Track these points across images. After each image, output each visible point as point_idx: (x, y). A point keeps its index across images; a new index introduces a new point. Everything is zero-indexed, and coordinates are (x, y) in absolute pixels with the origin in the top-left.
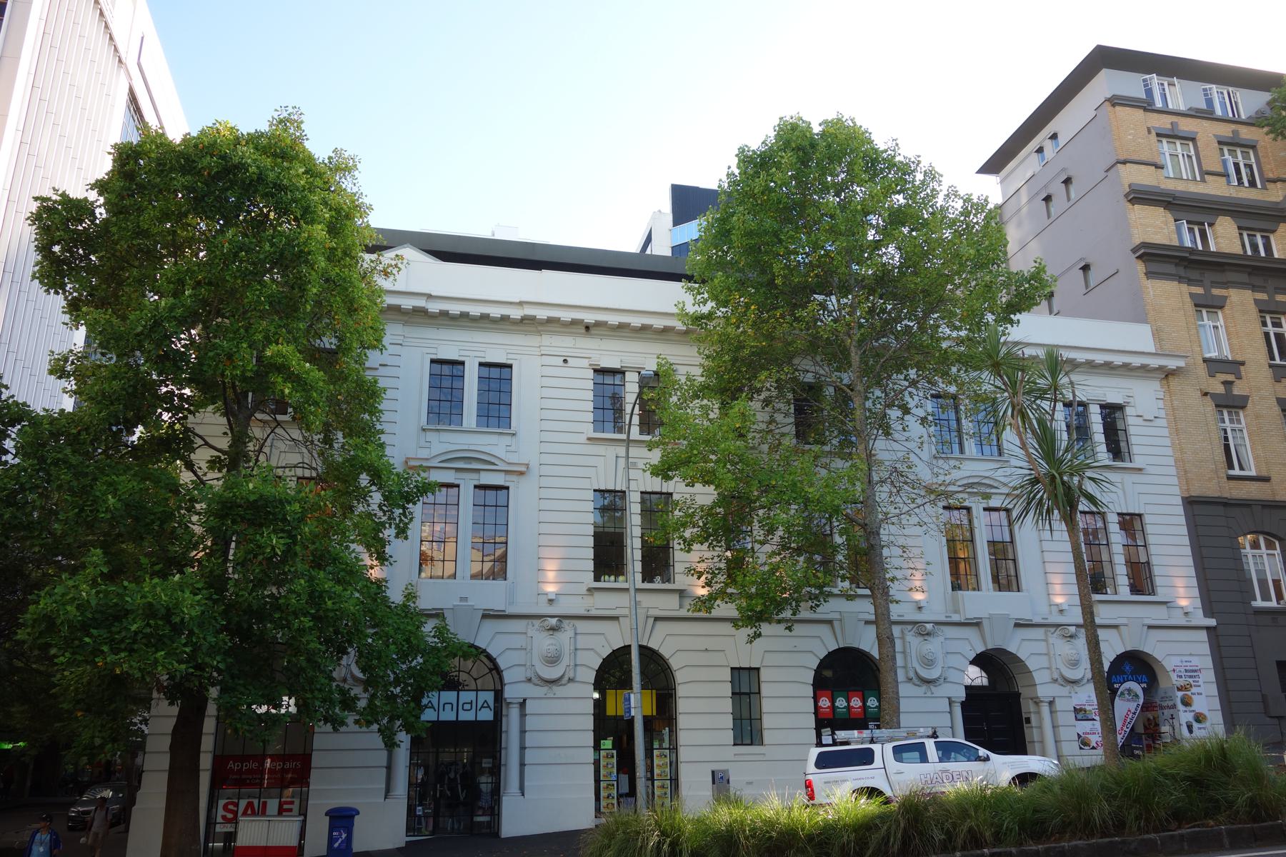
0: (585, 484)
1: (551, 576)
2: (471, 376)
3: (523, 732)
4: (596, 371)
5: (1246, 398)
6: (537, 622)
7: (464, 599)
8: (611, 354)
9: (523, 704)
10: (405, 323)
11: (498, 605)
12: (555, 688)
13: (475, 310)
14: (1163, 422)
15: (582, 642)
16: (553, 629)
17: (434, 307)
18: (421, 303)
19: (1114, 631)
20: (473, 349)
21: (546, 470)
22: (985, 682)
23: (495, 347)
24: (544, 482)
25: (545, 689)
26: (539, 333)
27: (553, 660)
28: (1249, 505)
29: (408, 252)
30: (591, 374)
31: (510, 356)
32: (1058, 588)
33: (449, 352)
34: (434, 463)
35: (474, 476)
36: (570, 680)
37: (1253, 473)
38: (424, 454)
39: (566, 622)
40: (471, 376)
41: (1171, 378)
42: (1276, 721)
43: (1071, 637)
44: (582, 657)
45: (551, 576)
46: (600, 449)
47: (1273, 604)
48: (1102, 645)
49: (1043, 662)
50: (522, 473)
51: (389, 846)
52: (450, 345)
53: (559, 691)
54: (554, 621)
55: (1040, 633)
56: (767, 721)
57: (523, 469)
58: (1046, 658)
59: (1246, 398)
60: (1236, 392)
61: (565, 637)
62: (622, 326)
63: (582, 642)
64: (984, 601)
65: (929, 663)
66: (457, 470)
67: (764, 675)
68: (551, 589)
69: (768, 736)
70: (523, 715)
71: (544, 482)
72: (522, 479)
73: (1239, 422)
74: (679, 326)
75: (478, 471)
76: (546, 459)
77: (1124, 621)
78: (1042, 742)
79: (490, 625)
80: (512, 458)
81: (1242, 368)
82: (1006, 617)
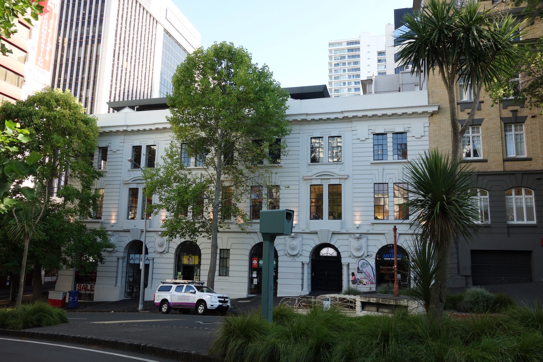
1: (114, 217)
2: (144, 151)
4: (374, 134)
5: (482, 120)
6: (352, 235)
7: (135, 226)
8: (380, 127)
9: (348, 265)
10: (300, 125)
11: (337, 229)
12: (163, 255)
13: (141, 128)
14: (427, 138)
15: (370, 243)
17: (129, 129)
19: (255, 234)
20: (144, 141)
21: (355, 177)
22: (321, 255)
23: (398, 126)
26: (351, 122)
27: (359, 250)
28: (514, 174)
30: (372, 136)
31: (340, 133)
32: (358, 218)
33: (137, 144)
34: (130, 182)
35: (310, 181)
38: (309, 174)
40: (144, 151)
44: (305, 247)
45: (114, 217)
46: (376, 167)
47: (525, 222)
49: (346, 248)
50: (346, 179)
51: (114, 300)
52: (137, 141)
53: (164, 256)
54: (358, 235)
55: (346, 237)
56: (231, 268)
57: (346, 177)
58: (283, 245)
61: (363, 241)
62: (383, 115)
63: (305, 242)
64: (326, 224)
65: (293, 249)
67: (231, 252)
68: (358, 223)
69: (230, 273)
73: (478, 132)
74: (169, 126)
75: (329, 179)
76: (355, 172)
77: (387, 232)
79: (337, 237)
80: (342, 173)
82: (329, 231)
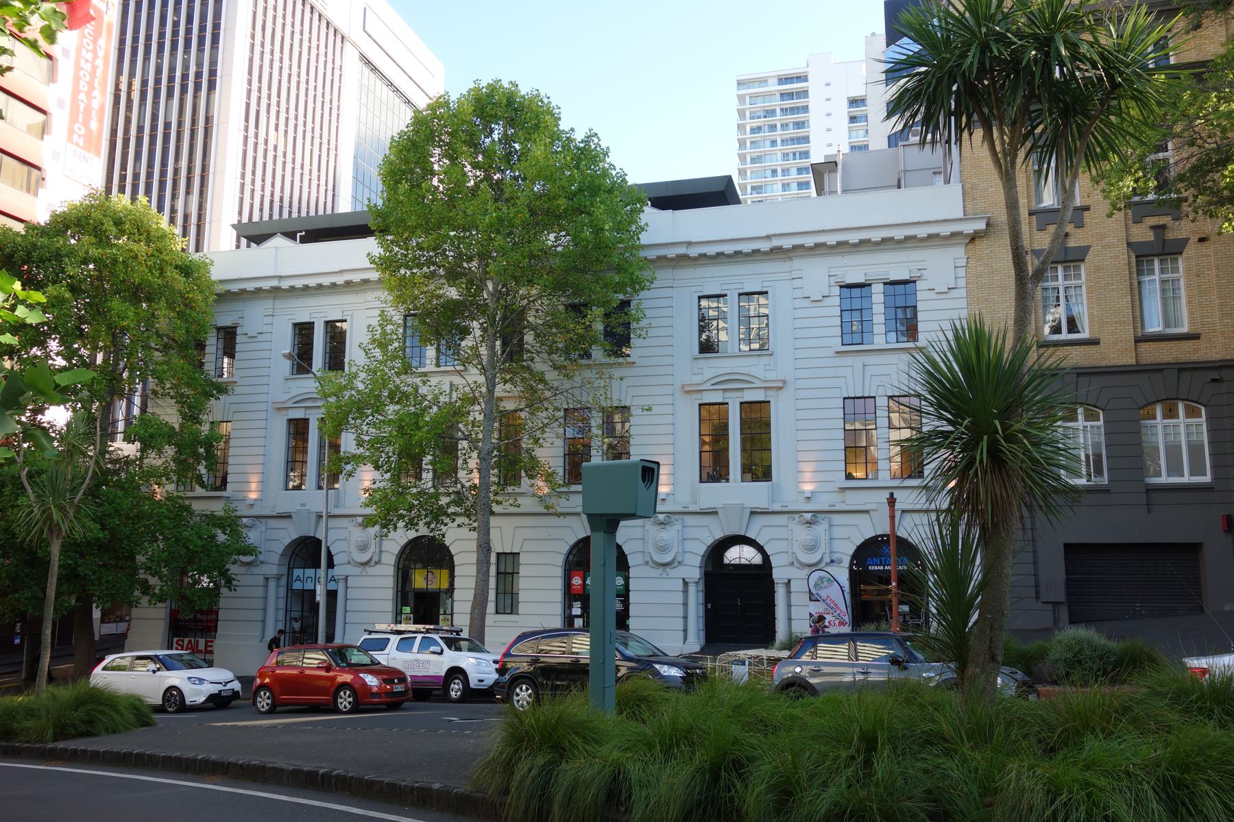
0: (836, 393)
1: (254, 486)
3: (685, 604)
4: (841, 287)
6: (796, 516)
8: (855, 269)
10: (674, 267)
11: (763, 504)
12: (668, 569)
14: (963, 293)
15: (837, 532)
16: (810, 523)
17: (285, 285)
18: (275, 283)
20: (318, 312)
22: (726, 561)
23: (897, 266)
24: (802, 394)
25: (360, 569)
26: (790, 258)
27: (812, 548)
28: (1161, 370)
29: (279, 241)
31: (765, 284)
32: (808, 476)
33: (303, 318)
34: (290, 404)
36: (376, 563)
37: (1185, 329)
39: (674, 517)
41: (977, 242)
42: (1050, 607)
43: (661, 523)
44: (689, 546)
45: (254, 486)
46: (849, 360)
47: (1186, 479)
48: (492, 531)
50: (781, 388)
53: (370, 570)
54: (808, 516)
55: (782, 519)
57: (780, 384)
59: (1085, 250)
60: (1170, 236)
61: (821, 529)
63: (689, 533)
64: (737, 492)
66: (725, 390)
67: (523, 559)
68: (808, 488)
70: (789, 592)
71: (802, 394)
72: (780, 392)
75: (742, 389)
78: (277, 609)
79: (760, 521)
80: (771, 375)
81: (1086, 214)
